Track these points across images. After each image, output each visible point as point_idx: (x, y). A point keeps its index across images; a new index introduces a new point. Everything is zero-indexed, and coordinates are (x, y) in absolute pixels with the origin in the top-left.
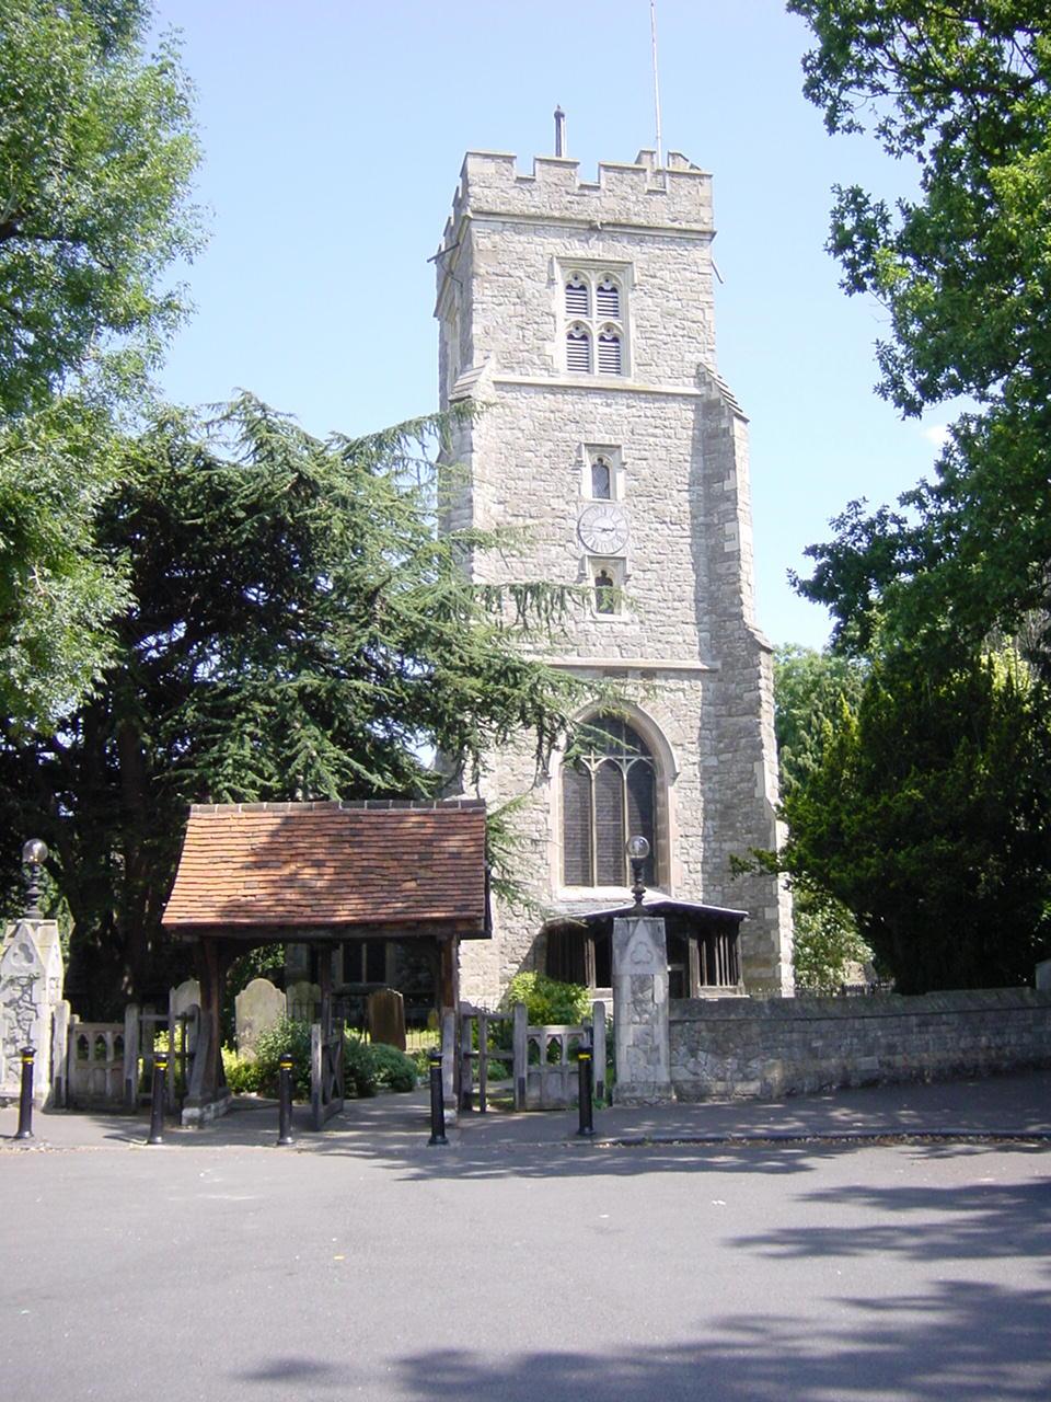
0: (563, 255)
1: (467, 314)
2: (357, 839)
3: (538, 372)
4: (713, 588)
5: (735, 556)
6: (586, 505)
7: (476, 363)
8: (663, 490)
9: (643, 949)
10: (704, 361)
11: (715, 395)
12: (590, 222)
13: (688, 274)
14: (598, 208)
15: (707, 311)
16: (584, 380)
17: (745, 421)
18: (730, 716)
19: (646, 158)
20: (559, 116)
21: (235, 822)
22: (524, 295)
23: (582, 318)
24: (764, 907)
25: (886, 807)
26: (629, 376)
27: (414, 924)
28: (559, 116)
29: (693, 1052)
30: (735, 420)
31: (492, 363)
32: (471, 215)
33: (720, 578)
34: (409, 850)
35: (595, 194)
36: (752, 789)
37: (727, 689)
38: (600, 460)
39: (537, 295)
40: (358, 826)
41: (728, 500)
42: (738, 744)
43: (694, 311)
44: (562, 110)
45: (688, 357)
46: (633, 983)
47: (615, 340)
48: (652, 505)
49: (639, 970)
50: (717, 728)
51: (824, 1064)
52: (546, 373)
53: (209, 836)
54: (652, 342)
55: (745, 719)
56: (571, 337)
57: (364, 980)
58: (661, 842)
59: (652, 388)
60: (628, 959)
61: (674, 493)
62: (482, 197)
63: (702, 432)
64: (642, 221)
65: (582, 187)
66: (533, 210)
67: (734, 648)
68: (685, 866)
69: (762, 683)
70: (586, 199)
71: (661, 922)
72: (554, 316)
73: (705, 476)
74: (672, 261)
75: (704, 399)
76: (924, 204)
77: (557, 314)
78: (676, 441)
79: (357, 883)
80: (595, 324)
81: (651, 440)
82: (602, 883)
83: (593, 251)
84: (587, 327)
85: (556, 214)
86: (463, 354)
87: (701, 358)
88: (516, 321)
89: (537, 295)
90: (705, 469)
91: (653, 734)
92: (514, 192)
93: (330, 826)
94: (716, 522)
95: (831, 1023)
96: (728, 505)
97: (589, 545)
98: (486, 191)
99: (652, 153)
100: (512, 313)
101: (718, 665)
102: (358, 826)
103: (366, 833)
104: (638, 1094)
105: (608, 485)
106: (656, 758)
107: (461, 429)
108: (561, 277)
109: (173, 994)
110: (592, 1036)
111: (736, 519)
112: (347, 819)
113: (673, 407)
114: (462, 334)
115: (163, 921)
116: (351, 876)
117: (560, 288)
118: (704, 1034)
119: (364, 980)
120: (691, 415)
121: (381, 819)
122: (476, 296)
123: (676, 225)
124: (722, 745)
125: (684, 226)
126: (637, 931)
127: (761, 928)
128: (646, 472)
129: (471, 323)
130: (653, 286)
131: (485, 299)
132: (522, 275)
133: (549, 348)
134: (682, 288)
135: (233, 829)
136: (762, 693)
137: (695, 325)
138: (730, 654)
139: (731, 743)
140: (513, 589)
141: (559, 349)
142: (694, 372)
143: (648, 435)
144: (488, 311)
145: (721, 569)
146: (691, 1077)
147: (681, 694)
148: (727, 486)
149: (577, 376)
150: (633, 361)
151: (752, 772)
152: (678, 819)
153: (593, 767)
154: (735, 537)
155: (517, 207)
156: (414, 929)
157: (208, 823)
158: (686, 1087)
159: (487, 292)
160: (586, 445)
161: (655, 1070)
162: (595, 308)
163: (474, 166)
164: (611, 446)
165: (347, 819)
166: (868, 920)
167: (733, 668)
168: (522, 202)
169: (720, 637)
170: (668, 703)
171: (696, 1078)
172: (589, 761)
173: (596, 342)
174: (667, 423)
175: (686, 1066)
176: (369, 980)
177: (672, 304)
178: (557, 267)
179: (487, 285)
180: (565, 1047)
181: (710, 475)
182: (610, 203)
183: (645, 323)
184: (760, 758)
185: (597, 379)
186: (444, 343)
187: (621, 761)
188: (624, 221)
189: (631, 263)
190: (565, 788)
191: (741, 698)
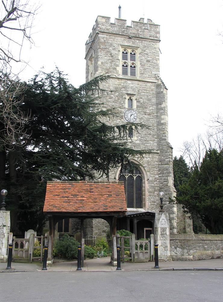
2: (92, 191)
5: (164, 124)
6: (126, 110)
9: (163, 221)
11: (160, 82)
16: (126, 77)
19: (142, 20)
20: (120, 8)
21: (59, 186)
25: (211, 188)
27: (109, 213)
28: (120, 8)
29: (176, 248)
34: (105, 194)
35: (131, 29)
37: (161, 158)
38: (130, 98)
39: (115, 55)
40: (92, 187)
46: (161, 229)
49: (163, 226)
50: (159, 168)
51: (207, 252)
53: (52, 189)
56: (123, 66)
57: (63, 231)
59: (144, 80)
60: (160, 223)
65: (127, 26)
66: (115, 32)
68: (150, 203)
70: (128, 30)
73: (157, 103)
75: (157, 83)
77: (120, 60)
79: (93, 202)
80: (129, 63)
85: (120, 33)
86: (95, 69)
89: (115, 55)
90: (156, 101)
92: (110, 27)
93: (84, 187)
95: (209, 241)
97: (127, 120)
98: (103, 27)
99: (143, 19)
102: (92, 187)
103: (94, 189)
104: (162, 258)
105: (132, 104)
108: (122, 50)
109: (26, 233)
110: (150, 243)
112: (89, 186)
113: (149, 84)
115: (44, 211)
116: (91, 200)
118: (178, 243)
119: (63, 231)
121: (97, 186)
123: (151, 38)
124: (159, 172)
125: (152, 38)
126: (162, 216)
131: (102, 55)
133: (118, 68)
135: (59, 187)
140: (118, 127)
141: (120, 69)
146: (175, 254)
148: (162, 106)
149: (125, 76)
153: (127, 177)
155: (110, 31)
156: (109, 214)
157: (51, 186)
158: (174, 257)
159: (102, 53)
160: (127, 94)
161: (167, 252)
164: (133, 94)
165: (89, 186)
166: (204, 217)
167: (163, 153)
168: (111, 30)
171: (176, 255)
175: (174, 251)
176: (64, 232)
177: (149, 59)
179: (102, 51)
180: (144, 246)
181: (158, 103)
182: (134, 31)
186: (88, 66)
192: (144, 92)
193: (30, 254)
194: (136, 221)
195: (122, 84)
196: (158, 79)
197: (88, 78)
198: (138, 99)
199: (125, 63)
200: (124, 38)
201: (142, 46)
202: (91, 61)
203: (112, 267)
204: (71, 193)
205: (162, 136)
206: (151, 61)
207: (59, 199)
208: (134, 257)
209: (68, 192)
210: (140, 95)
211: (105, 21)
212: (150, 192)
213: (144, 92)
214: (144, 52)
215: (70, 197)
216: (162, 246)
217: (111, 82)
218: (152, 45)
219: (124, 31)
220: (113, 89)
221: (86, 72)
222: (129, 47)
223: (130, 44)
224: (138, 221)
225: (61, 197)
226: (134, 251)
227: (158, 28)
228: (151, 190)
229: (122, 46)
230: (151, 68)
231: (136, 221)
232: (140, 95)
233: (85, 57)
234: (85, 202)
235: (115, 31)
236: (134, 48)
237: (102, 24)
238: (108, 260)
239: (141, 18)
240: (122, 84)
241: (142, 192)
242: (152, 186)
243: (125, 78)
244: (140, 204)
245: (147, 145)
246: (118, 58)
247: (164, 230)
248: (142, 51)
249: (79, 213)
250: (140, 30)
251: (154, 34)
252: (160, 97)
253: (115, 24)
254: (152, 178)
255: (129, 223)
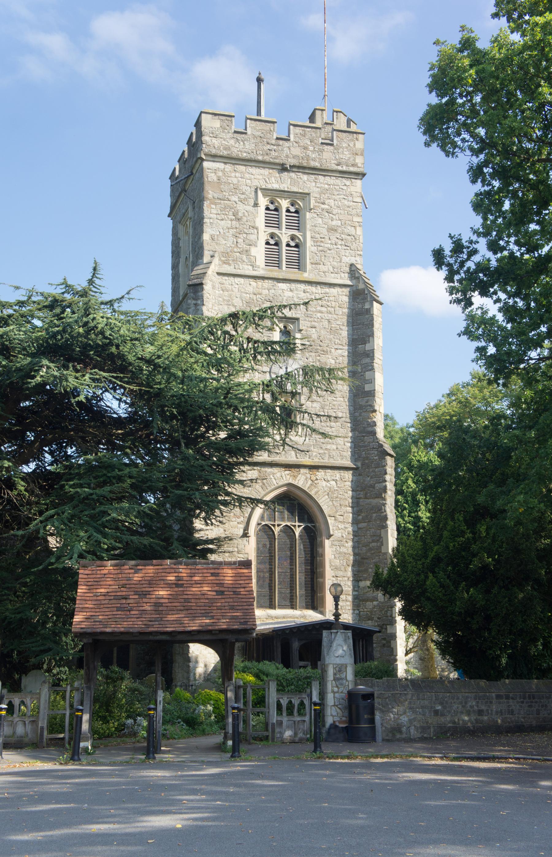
0: (264, 187)
1: (198, 225)
3: (246, 267)
4: (357, 414)
7: (206, 259)
8: (325, 349)
10: (354, 262)
11: (361, 286)
12: (283, 165)
13: (346, 202)
14: (290, 153)
15: (358, 228)
16: (275, 273)
17: (381, 304)
18: (366, 498)
20: (259, 80)
22: (237, 213)
23: (276, 231)
24: (386, 625)
26: (305, 271)
27: (217, 632)
30: (374, 303)
31: (216, 261)
32: (204, 157)
33: (361, 407)
35: (286, 144)
36: (380, 548)
37: (364, 481)
38: (285, 327)
39: (246, 214)
41: (368, 357)
42: (371, 517)
43: (349, 228)
44: (263, 76)
45: (345, 259)
47: (297, 246)
48: (318, 358)
50: (357, 506)
51: (443, 719)
52: (250, 268)
54: (320, 248)
55: (376, 500)
56: (267, 243)
58: (320, 580)
61: (333, 350)
62: (211, 143)
63: (353, 310)
64: (317, 164)
66: (245, 154)
67: (368, 454)
69: (388, 477)
70: (280, 148)
71: (350, 634)
72: (257, 229)
74: (336, 193)
75: (355, 289)
76: (476, 355)
78: (335, 316)
80: (285, 236)
81: (319, 315)
82: (281, 607)
83: (284, 185)
84: (279, 237)
85: (260, 158)
87: (353, 260)
88: (232, 231)
89: (246, 214)
91: (316, 509)
92: (232, 142)
94: (360, 371)
96: (367, 360)
98: (214, 140)
99: (322, 110)
100: (229, 226)
101: (359, 464)
106: (317, 525)
107: (196, 305)
108: (263, 202)
111: (372, 369)
113: (334, 291)
114: (194, 237)
116: (179, 604)
117: (262, 210)
120: (346, 299)
122: (206, 213)
123: (340, 168)
124: (360, 517)
125: (345, 168)
127: (384, 639)
128: (315, 336)
129: (203, 232)
130: (323, 210)
131: (212, 216)
132: (237, 200)
133: (254, 251)
134: (342, 212)
136: (387, 483)
137: (349, 237)
138: (367, 458)
139: (367, 516)
141: (259, 252)
142: (347, 269)
143: (316, 311)
144: (216, 228)
145: (362, 402)
147: (334, 483)
148: (368, 347)
150: (308, 261)
151: (380, 537)
152: (331, 566)
154: (372, 381)
162: (284, 224)
163: (206, 121)
168: (240, 148)
169: (361, 447)
170: (326, 489)
172: (274, 525)
173: (284, 248)
174: (329, 304)
177: (334, 223)
178: (260, 193)
179: (213, 206)
182: (296, 151)
183: (317, 236)
184: (385, 527)
185: (285, 272)
187: (295, 526)
188: (305, 165)
189: (309, 194)
190: (258, 543)
191: (374, 487)
192: (321, 312)
193: (42, 728)
194: (296, 645)
195: (264, 291)
196: (357, 275)
197: (178, 270)
198: (306, 331)
199: (272, 236)
200: (271, 171)
201: (318, 189)
202: (185, 225)
203: (222, 754)
204: (132, 590)
205: (365, 425)
206: (340, 230)
207: (106, 602)
208: (273, 731)
209: (127, 586)
210: (310, 319)
211: (219, 126)
212: (336, 568)
213: (321, 312)
214: (323, 206)
215: (131, 597)
216: (337, 706)
217: (237, 286)
218: (343, 187)
219: (269, 151)
220: (241, 305)
221: (173, 252)
222: (283, 193)
223: (284, 187)
224: (303, 642)
225: (112, 598)
226: (274, 718)
227: (357, 139)
228: (337, 562)
229: (266, 191)
230: (340, 247)
231: (296, 645)
232: (310, 319)
233: (168, 211)
234: (166, 609)
235: (245, 152)
236: (295, 197)
237: (213, 133)
238: (218, 739)
239: (315, 109)
240: (265, 292)
241: (316, 569)
242: (340, 553)
243: (271, 276)
244: (314, 601)
245: (329, 447)
246: (254, 222)
247: (340, 669)
248: (317, 204)
249: (151, 633)
250: (311, 148)
251: (349, 156)
252: (363, 325)
253: (246, 133)
254: (342, 533)
255: (279, 650)
